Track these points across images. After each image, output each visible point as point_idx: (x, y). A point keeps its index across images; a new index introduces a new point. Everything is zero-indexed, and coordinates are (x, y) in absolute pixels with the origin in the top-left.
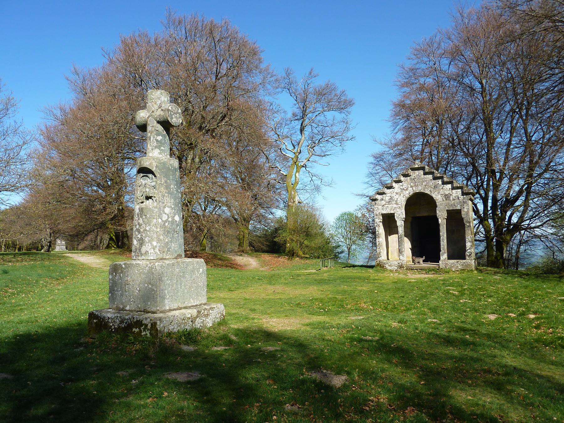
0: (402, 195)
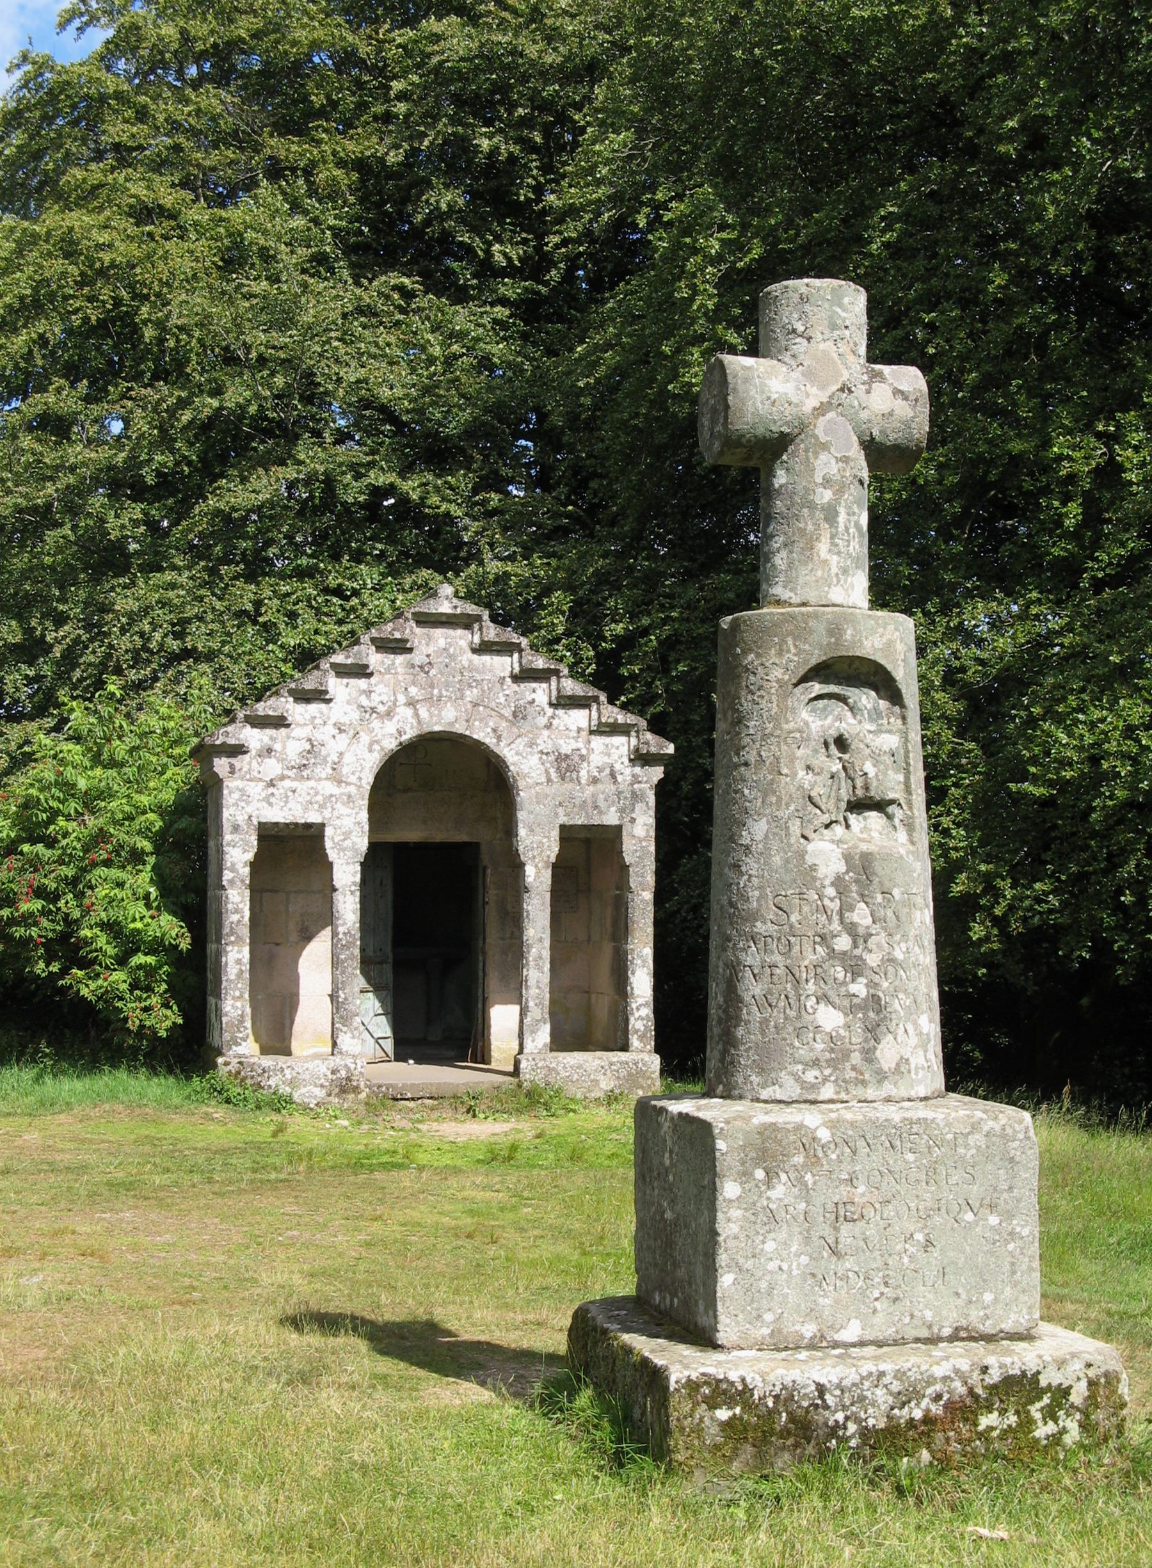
0: (365, 738)
